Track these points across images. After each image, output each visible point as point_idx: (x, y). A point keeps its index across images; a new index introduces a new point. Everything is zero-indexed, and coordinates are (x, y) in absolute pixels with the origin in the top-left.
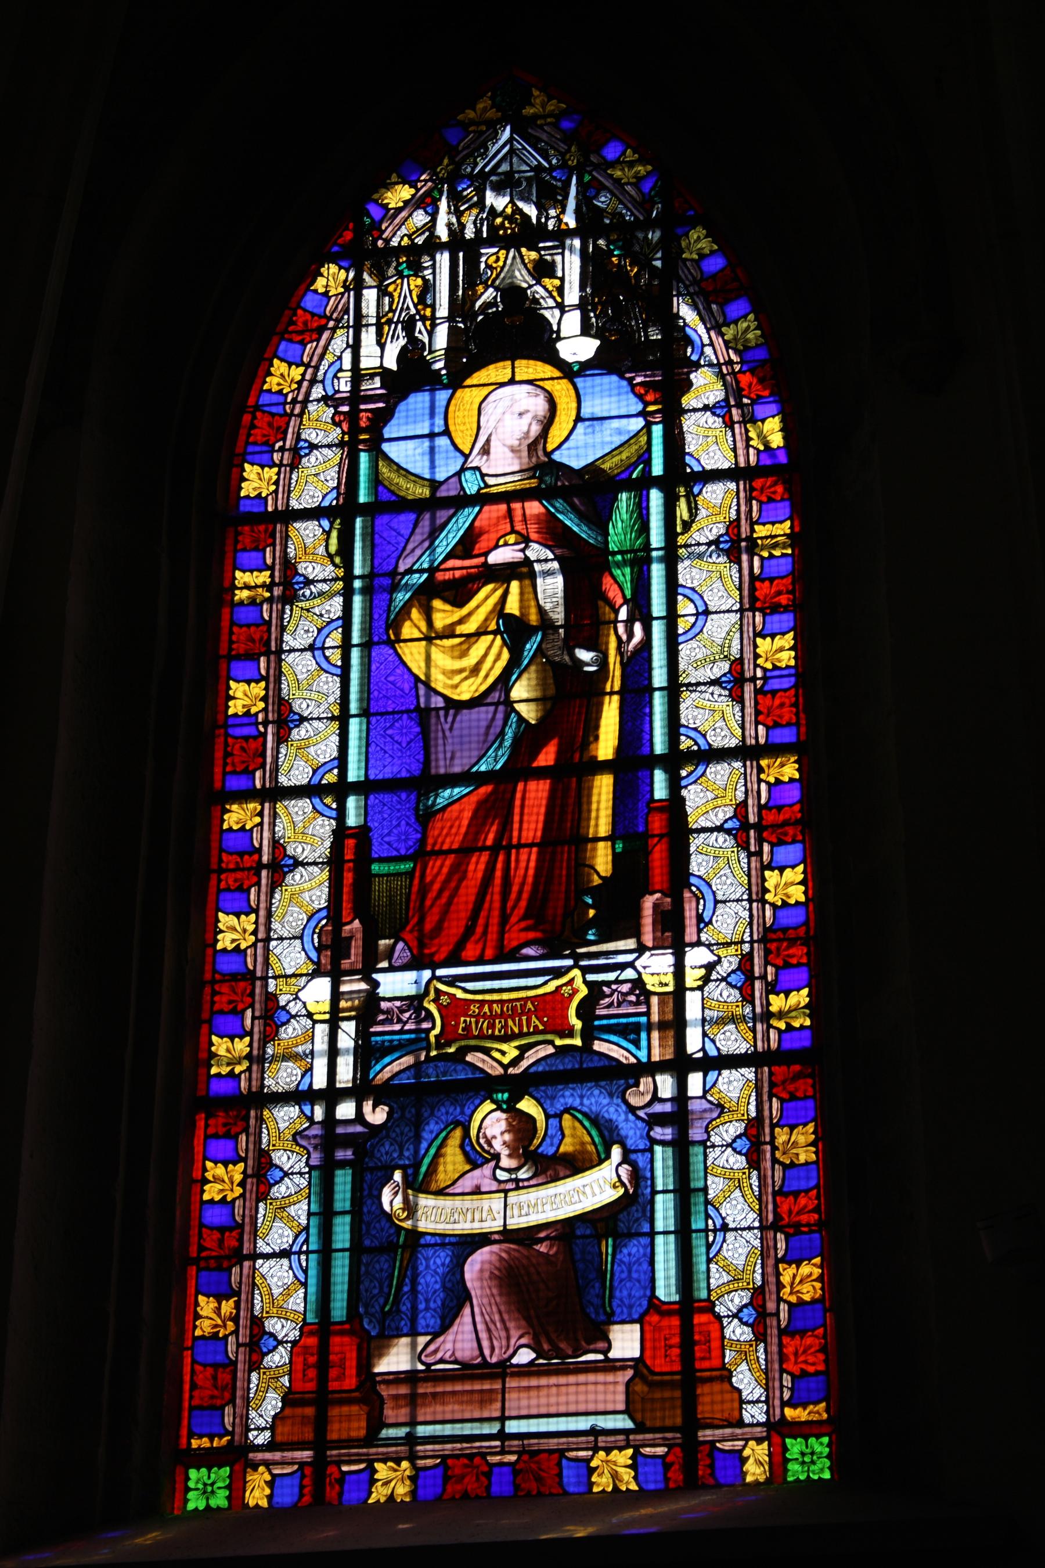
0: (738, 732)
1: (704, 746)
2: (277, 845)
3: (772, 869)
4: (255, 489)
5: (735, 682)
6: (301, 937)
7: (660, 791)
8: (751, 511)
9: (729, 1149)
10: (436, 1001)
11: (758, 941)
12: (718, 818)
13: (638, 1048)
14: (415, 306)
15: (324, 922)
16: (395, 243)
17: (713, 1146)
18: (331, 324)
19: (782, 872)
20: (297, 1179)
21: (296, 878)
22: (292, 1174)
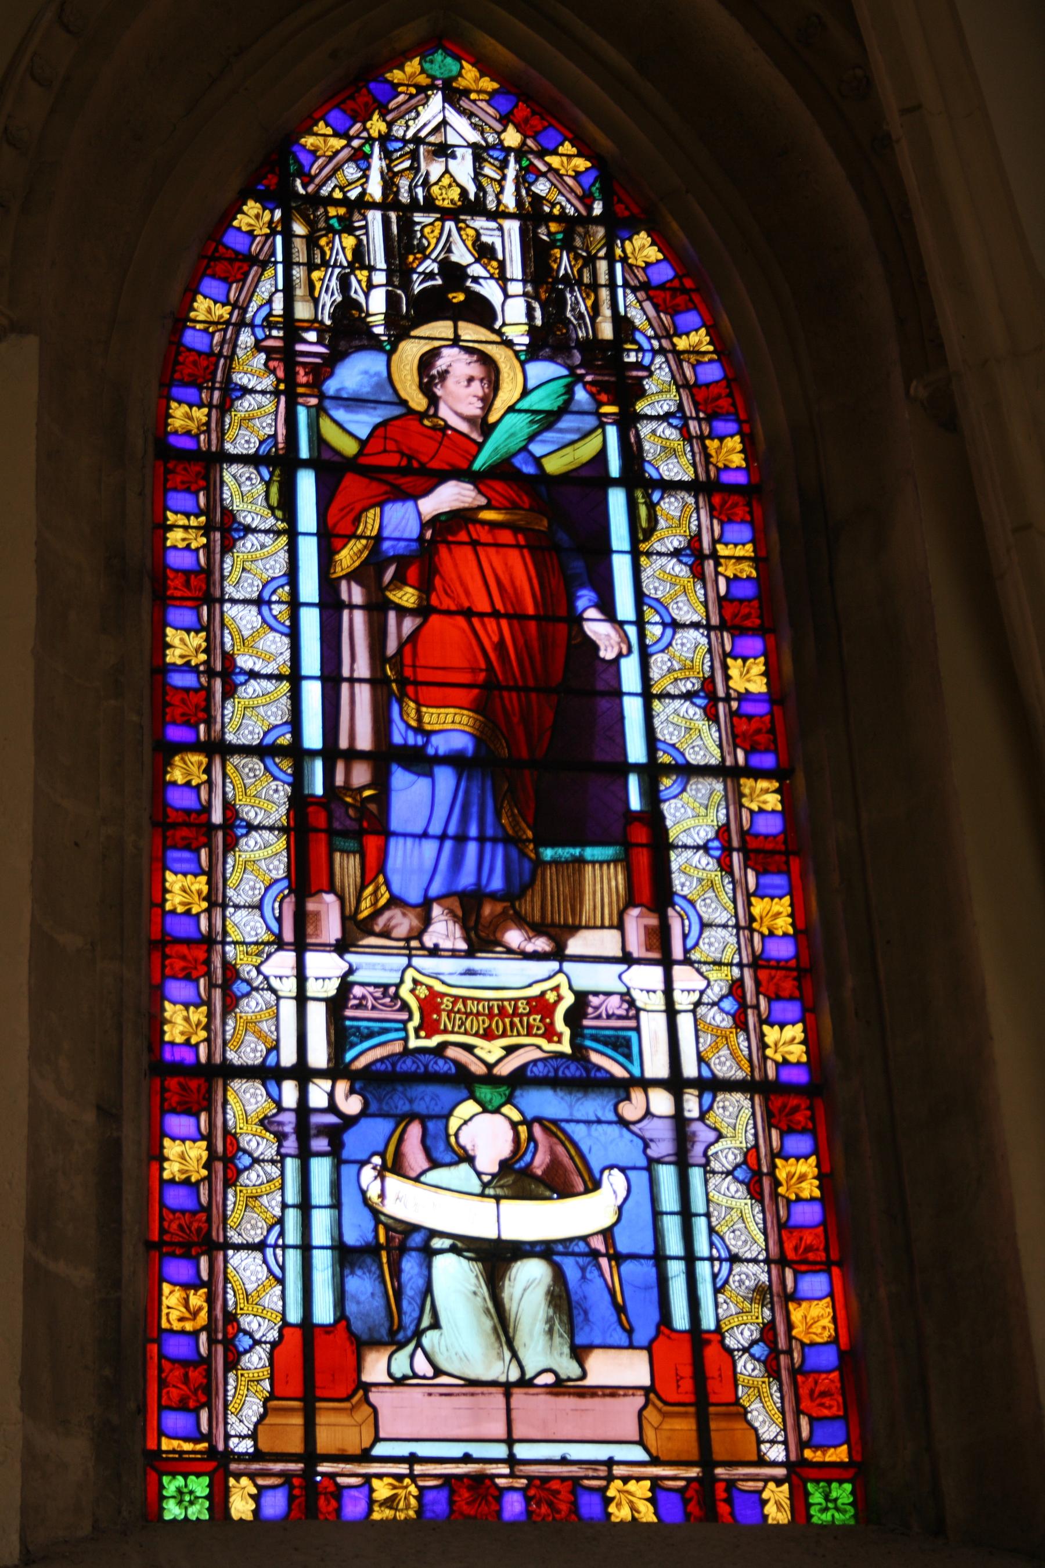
1: (681, 760)
2: (229, 807)
5: (708, 695)
11: (748, 966)
13: (631, 1061)
16: (325, 192)
17: (714, 1172)
19: (782, 1028)
20: (269, 1167)
21: (251, 844)
22: (263, 1161)
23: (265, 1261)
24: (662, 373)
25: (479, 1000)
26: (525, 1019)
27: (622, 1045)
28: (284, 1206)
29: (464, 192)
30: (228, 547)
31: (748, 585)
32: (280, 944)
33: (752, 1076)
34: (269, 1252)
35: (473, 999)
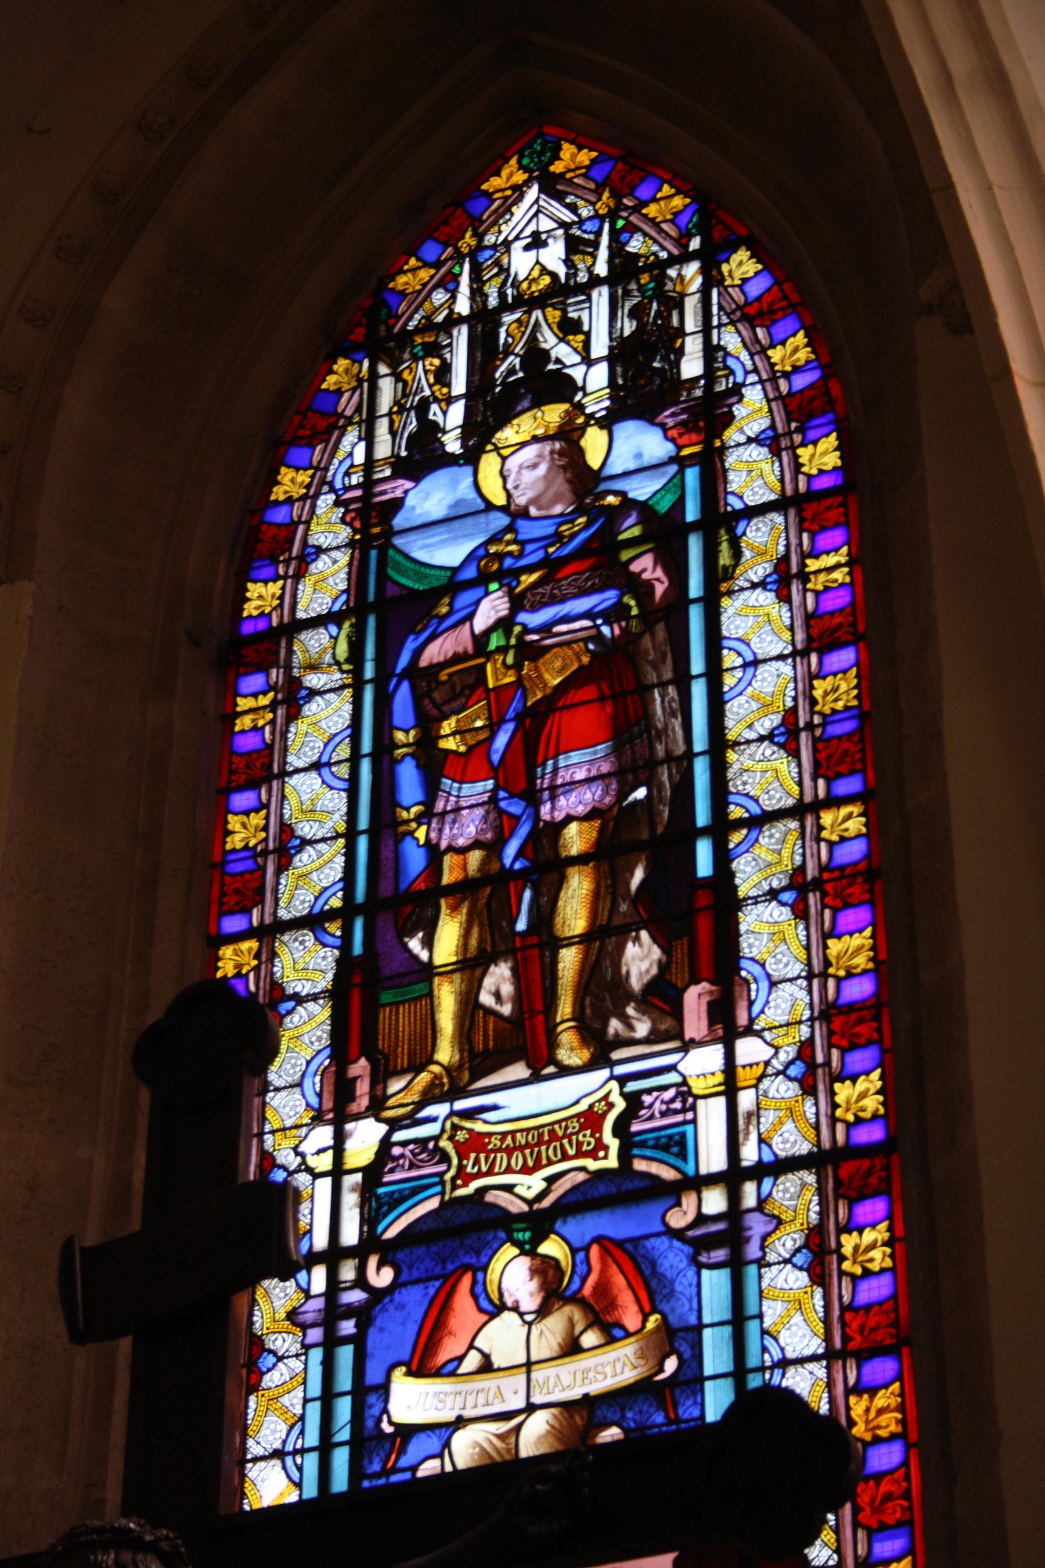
0: (795, 790)
3: (842, 1081)
4: (256, 608)
5: (787, 736)
6: (300, 1085)
7: (704, 864)
8: (801, 544)
9: (789, 1266)
10: (451, 1138)
12: (765, 726)
13: (685, 1159)
14: (430, 386)
15: (327, 1062)
18: (341, 422)
23: (284, 1468)
24: (754, 395)
25: (528, 1130)
26: (574, 1138)
27: (676, 1146)
28: (306, 1401)
29: (554, 276)
30: (294, 714)
31: (842, 592)
32: (318, 1119)
33: (818, 1144)
34: (289, 1460)
35: (521, 1131)
